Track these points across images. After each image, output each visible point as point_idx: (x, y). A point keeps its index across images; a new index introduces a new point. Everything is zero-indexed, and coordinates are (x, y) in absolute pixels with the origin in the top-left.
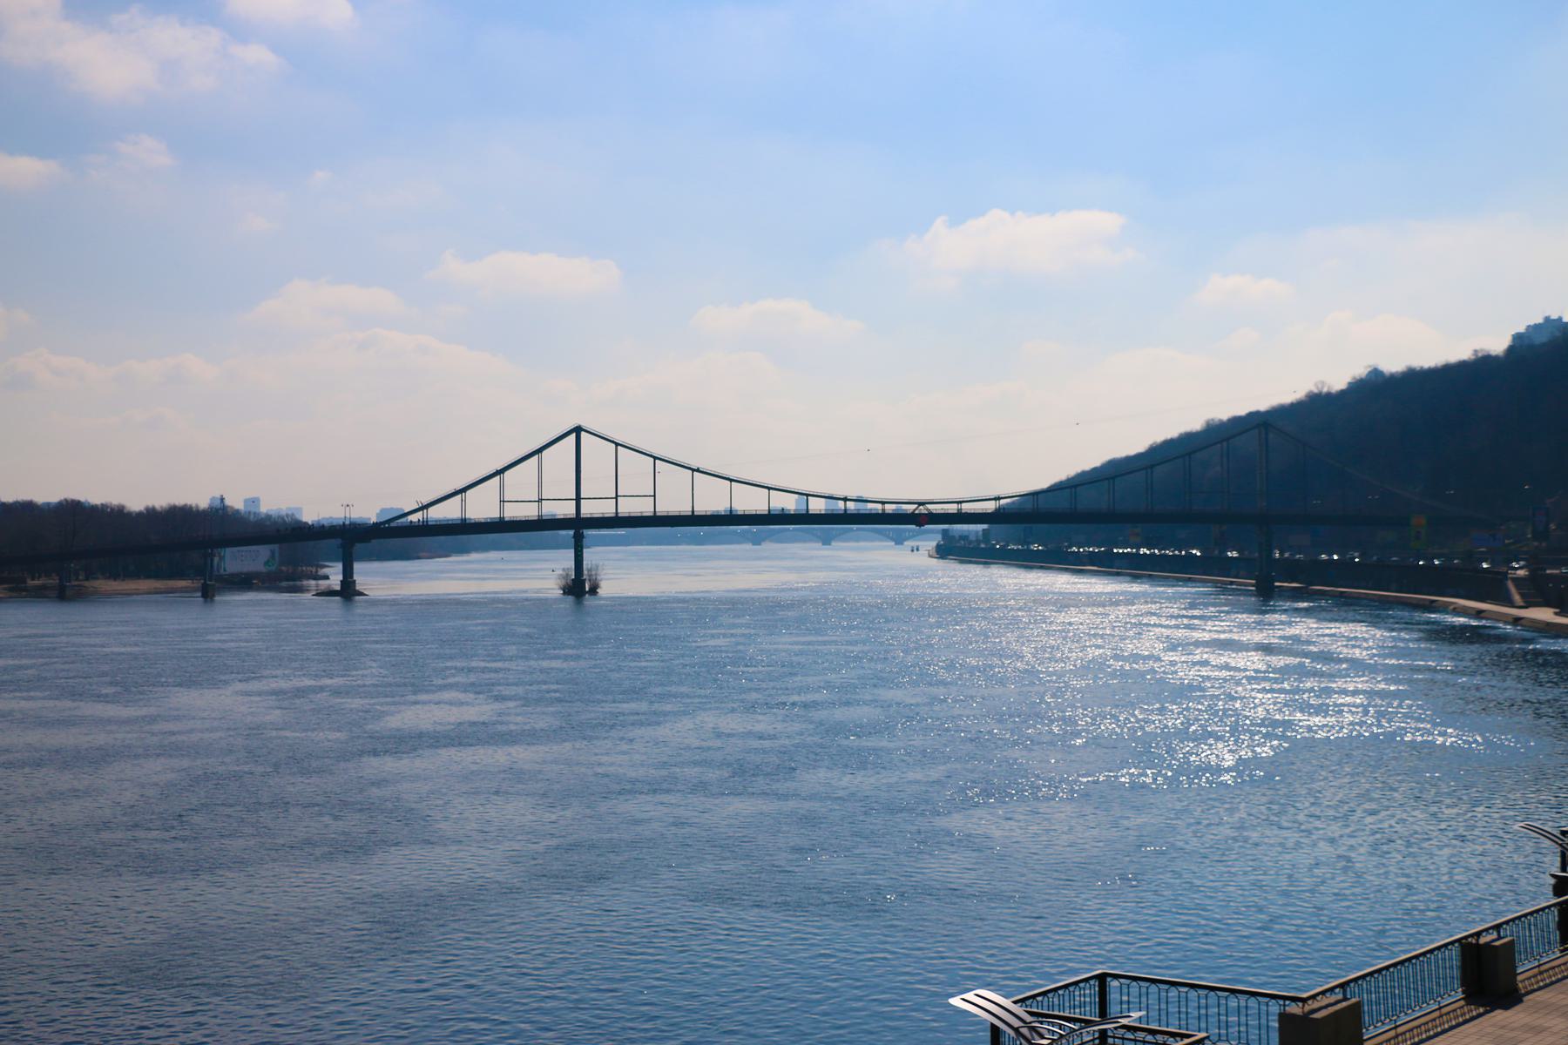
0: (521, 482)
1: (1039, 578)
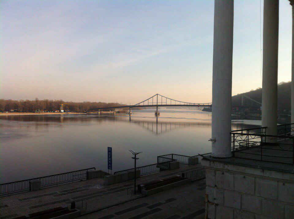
0: (150, 101)
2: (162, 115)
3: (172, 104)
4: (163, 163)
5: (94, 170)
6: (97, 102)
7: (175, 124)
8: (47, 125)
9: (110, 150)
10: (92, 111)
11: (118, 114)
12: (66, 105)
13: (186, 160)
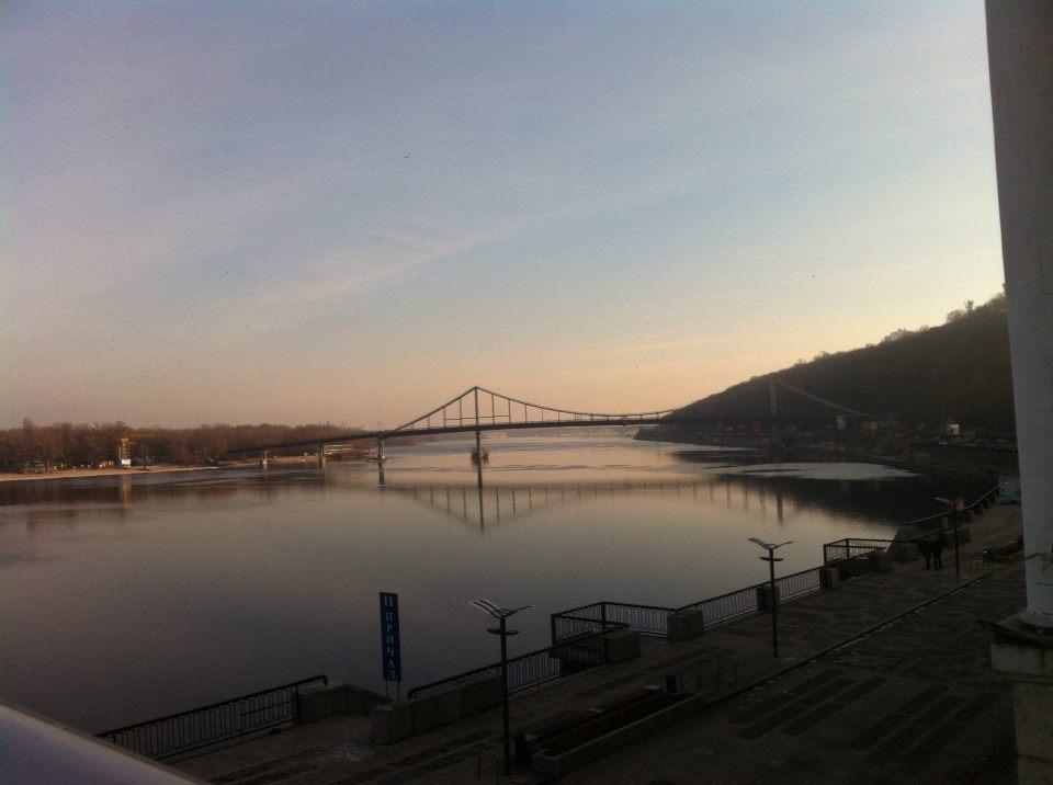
0: (453, 411)
1: (499, 436)
2: (495, 459)
3: (530, 420)
4: (574, 642)
5: (320, 685)
6: (256, 422)
7: (546, 488)
8: (70, 514)
9: (389, 604)
10: (238, 459)
11: (337, 463)
12: (139, 441)
13: (660, 624)
